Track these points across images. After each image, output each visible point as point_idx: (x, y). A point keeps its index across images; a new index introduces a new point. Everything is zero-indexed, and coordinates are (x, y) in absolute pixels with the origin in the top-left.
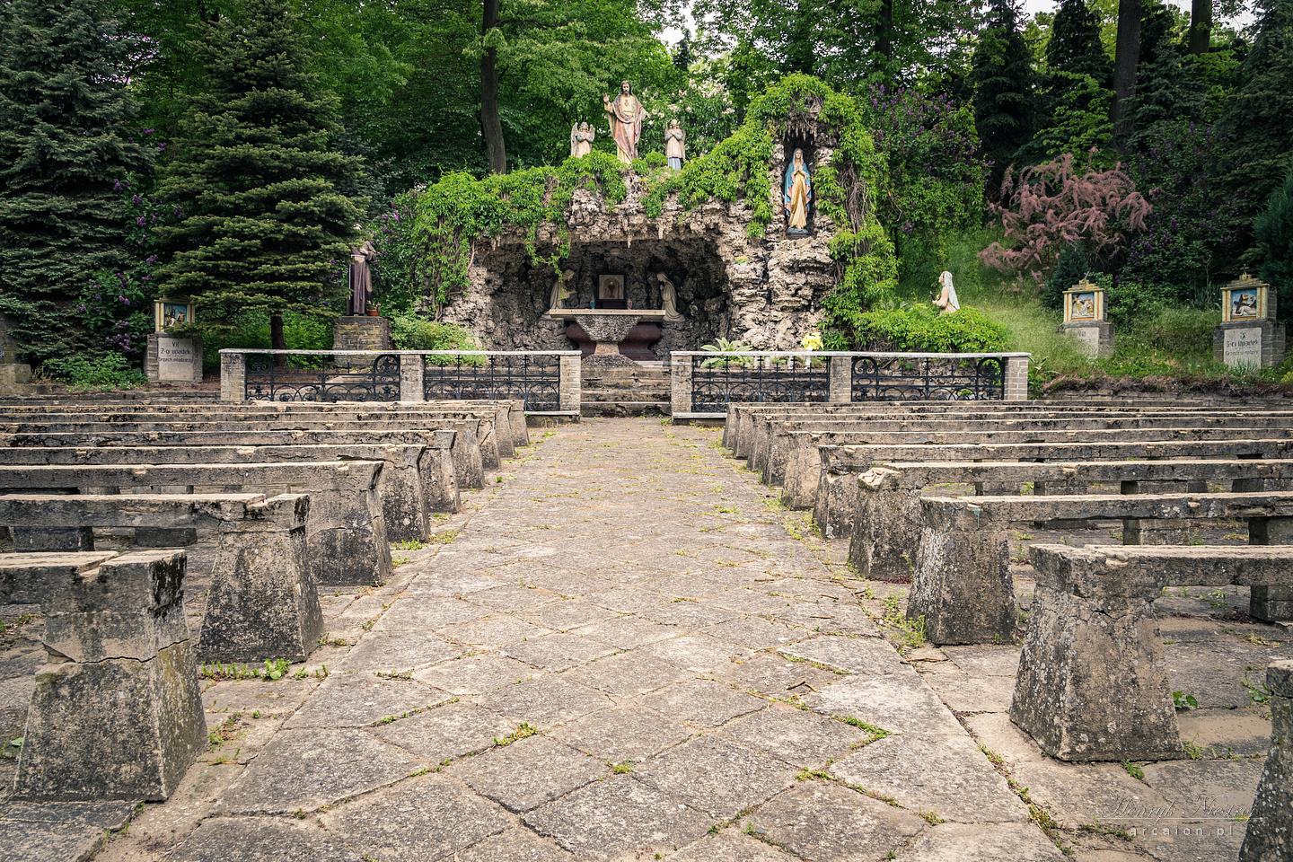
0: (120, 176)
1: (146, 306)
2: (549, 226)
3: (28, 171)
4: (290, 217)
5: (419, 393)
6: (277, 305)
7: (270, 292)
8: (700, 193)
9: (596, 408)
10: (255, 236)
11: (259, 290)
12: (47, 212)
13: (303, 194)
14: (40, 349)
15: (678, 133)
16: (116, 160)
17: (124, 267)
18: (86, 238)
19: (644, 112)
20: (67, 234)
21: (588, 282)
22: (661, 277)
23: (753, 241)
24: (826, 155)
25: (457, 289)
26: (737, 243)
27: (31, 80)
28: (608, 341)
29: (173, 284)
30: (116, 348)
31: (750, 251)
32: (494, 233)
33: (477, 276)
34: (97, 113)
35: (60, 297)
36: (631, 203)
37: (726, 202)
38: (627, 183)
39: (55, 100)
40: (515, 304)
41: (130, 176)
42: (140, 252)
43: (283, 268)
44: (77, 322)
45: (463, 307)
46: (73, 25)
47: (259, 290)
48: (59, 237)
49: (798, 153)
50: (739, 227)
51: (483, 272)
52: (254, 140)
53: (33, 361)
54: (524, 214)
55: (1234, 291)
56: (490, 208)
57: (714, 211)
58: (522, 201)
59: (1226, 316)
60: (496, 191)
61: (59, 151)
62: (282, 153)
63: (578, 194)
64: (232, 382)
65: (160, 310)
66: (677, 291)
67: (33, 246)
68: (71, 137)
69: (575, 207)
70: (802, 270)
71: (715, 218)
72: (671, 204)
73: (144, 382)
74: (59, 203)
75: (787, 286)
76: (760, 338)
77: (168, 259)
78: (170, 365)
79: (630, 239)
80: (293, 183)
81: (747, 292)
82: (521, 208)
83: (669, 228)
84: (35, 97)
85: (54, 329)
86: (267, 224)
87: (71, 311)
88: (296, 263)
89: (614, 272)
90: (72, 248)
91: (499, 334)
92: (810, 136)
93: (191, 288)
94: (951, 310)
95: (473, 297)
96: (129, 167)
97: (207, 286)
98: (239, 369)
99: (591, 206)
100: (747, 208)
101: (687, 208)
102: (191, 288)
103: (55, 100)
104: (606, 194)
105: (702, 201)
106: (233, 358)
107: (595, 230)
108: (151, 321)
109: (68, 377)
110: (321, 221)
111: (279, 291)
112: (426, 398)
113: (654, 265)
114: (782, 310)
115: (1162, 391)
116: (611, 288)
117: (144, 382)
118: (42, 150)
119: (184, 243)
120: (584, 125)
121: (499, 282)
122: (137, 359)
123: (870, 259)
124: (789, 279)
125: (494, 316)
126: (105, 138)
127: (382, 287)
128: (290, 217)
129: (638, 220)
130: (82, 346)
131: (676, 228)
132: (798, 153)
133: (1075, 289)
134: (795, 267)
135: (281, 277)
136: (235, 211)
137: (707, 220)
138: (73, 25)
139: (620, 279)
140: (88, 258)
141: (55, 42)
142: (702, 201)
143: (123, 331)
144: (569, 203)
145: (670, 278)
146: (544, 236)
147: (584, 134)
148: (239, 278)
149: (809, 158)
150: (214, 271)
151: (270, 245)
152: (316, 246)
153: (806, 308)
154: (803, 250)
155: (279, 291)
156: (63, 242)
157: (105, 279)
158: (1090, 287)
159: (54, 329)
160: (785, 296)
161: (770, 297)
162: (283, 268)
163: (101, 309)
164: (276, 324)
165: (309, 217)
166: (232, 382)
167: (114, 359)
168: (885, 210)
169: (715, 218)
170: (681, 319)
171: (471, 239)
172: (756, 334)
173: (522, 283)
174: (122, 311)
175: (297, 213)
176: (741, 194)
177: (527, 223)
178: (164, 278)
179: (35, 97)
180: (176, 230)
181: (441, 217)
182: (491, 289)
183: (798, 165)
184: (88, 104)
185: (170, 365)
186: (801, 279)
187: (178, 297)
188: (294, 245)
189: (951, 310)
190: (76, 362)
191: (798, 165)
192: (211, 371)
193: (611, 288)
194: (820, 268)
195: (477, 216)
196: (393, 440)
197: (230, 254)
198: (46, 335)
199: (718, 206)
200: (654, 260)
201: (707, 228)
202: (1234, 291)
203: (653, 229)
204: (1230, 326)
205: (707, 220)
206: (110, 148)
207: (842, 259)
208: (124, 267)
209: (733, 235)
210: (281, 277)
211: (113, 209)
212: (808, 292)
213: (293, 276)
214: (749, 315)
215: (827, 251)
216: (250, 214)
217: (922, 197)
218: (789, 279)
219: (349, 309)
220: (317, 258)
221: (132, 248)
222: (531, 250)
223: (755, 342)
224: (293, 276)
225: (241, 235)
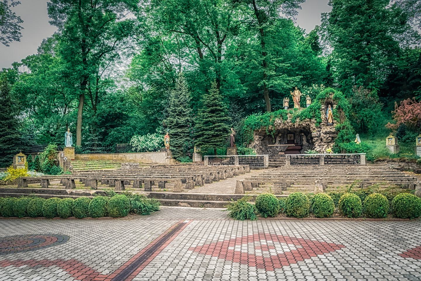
0: (189, 124)
1: (193, 148)
2: (271, 126)
3: (175, 125)
4: (217, 131)
5: (238, 163)
6: (214, 147)
7: (213, 145)
8: (304, 117)
9: (274, 166)
10: (210, 135)
11: (211, 145)
12: (177, 132)
13: (219, 126)
14: (176, 156)
15: (309, 98)
16: (188, 121)
17: (189, 141)
18: (183, 136)
19: (301, 94)
20: (180, 135)
21: (286, 136)
22: (303, 134)
23: (317, 127)
24: (335, 106)
25: (251, 141)
26: (314, 128)
27: (175, 109)
28: (281, 151)
29: (197, 144)
30: (188, 155)
31: (317, 129)
32: (259, 128)
33: (256, 137)
34: (185, 113)
35: (179, 146)
36: (289, 120)
37: (310, 119)
38: (288, 116)
39: (179, 112)
40: (268, 142)
41: (190, 124)
42: (192, 138)
43: (215, 140)
44: (182, 151)
45: (253, 144)
46: (182, 99)
47: (211, 145)
48: (179, 136)
49: (329, 106)
50: (314, 124)
51: (258, 136)
52: (211, 117)
53: (175, 158)
54: (266, 124)
55: (418, 138)
56: (258, 123)
57: (307, 121)
58: (265, 121)
59: (417, 144)
60: (260, 119)
61: (179, 121)
62: (216, 119)
63: (276, 119)
64: (206, 162)
65: (195, 148)
66: (307, 137)
67: (175, 138)
68: (181, 118)
69: (276, 122)
70: (328, 133)
71: (308, 123)
72: (298, 120)
73: (192, 161)
74: (179, 130)
75: (325, 137)
76: (318, 149)
77: (196, 139)
78: (197, 158)
79: (289, 128)
80: (217, 124)
81: (315, 139)
82: (265, 123)
83: (298, 125)
84: (176, 112)
85: (178, 152)
86: (212, 133)
87: (181, 149)
88: (218, 139)
89: (292, 133)
90: (181, 138)
91: (263, 149)
92: (331, 102)
93: (200, 144)
94: (358, 143)
95: (256, 142)
96: (190, 122)
97: (203, 144)
98: (207, 159)
99: (279, 122)
100: (315, 120)
101: (301, 121)
102: (200, 144)
103: (179, 112)
104: (283, 119)
105: (305, 119)
106: (206, 157)
107: (281, 127)
108: (193, 150)
109: (180, 161)
110: (222, 131)
111: (215, 145)
112: (239, 164)
113: (301, 131)
114: (325, 142)
115: (396, 162)
116: (291, 137)
117: (192, 161)
118: (177, 121)
119: (199, 136)
120: (286, 98)
121: (263, 138)
122: (191, 157)
123: (344, 131)
124: (325, 136)
125: (262, 145)
126: (187, 118)
127: (237, 141)
128: (217, 131)
129: (290, 124)
130: (183, 155)
131: (299, 125)
132: (329, 106)
133: (388, 137)
134: (326, 133)
135: (215, 142)
136: (206, 130)
137: (306, 123)
138: (182, 99)
139: (293, 135)
140: (184, 140)
141: (179, 102)
142: (305, 119)
143: (189, 152)
144: (274, 121)
145: (305, 134)
146: (270, 128)
147: (286, 100)
148: (208, 142)
149: (332, 107)
150: (204, 141)
151: (213, 136)
152: (221, 136)
153: (330, 142)
154: (328, 129)
155: (215, 145)
156: (180, 137)
157: (186, 144)
158: (391, 137)
159: (178, 152)
160: (324, 140)
161: (321, 140)
162: (215, 140)
163: (185, 149)
164: (215, 150)
165: (220, 130)
166: (206, 162)
167: (188, 158)
168: (351, 118)
169: (308, 123)
170: (308, 144)
171: (254, 130)
172: (318, 149)
173: (268, 138)
174: (189, 149)
175: (218, 130)
176: (314, 117)
177: (266, 126)
178: (196, 143)
179: (176, 112)
180: (198, 134)
181: (248, 126)
182: (261, 139)
183: (330, 108)
184: (184, 112)
185: (197, 158)
186: (328, 135)
187: (198, 146)
188: (217, 136)
189: (358, 143)
190: (182, 158)
191: (330, 108)
192: (203, 159)
193: (291, 137)
194: (334, 133)
195: (255, 125)
196: (101, 162)
197: (206, 138)
198: (177, 153)
199: (308, 120)
200: (301, 130)
201: (307, 125)
202: (418, 138)
203: (294, 125)
204: (418, 146)
205: (306, 123)
206: (188, 120)
207: (338, 130)
208: (189, 141)
209: (312, 126)
210: (215, 142)
211: (188, 130)
212: (330, 138)
213: (217, 142)
214: (317, 144)
215: (334, 129)
216: (210, 130)
217: (363, 114)
218: (325, 136)
219: (229, 146)
220: (221, 138)
221: (190, 137)
222: (267, 131)
223: (317, 150)
224: (217, 142)
225: (208, 135)
